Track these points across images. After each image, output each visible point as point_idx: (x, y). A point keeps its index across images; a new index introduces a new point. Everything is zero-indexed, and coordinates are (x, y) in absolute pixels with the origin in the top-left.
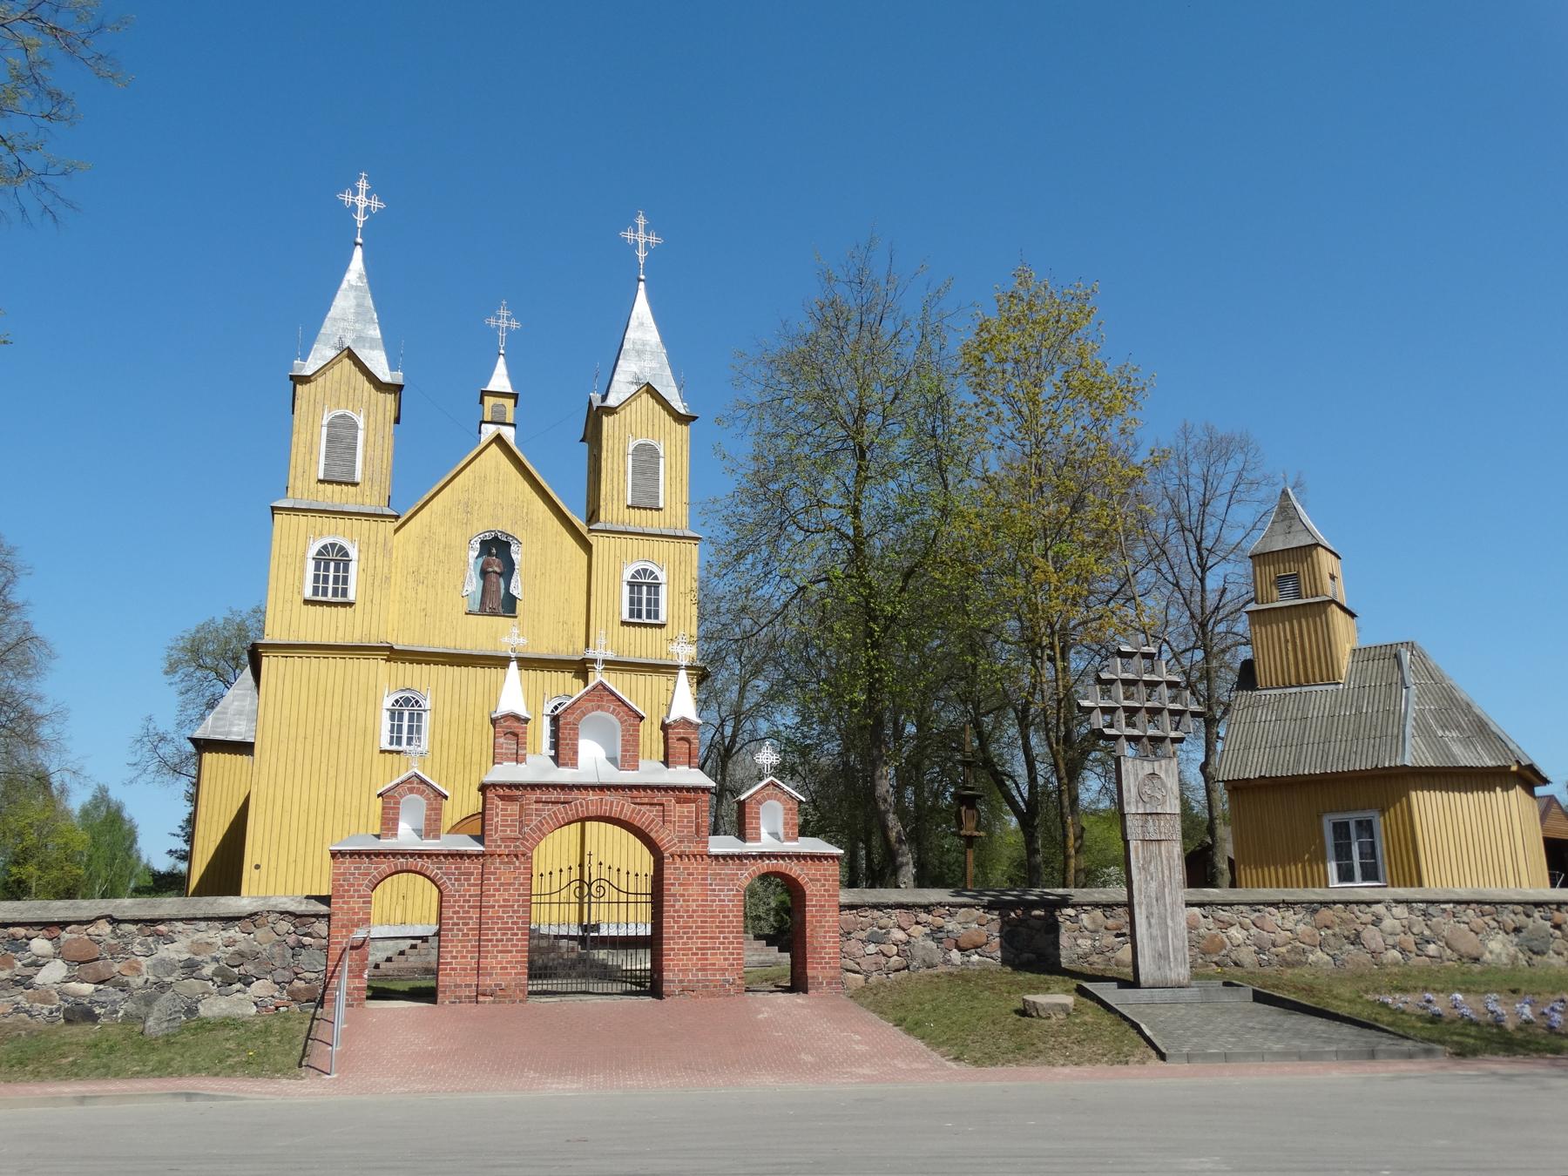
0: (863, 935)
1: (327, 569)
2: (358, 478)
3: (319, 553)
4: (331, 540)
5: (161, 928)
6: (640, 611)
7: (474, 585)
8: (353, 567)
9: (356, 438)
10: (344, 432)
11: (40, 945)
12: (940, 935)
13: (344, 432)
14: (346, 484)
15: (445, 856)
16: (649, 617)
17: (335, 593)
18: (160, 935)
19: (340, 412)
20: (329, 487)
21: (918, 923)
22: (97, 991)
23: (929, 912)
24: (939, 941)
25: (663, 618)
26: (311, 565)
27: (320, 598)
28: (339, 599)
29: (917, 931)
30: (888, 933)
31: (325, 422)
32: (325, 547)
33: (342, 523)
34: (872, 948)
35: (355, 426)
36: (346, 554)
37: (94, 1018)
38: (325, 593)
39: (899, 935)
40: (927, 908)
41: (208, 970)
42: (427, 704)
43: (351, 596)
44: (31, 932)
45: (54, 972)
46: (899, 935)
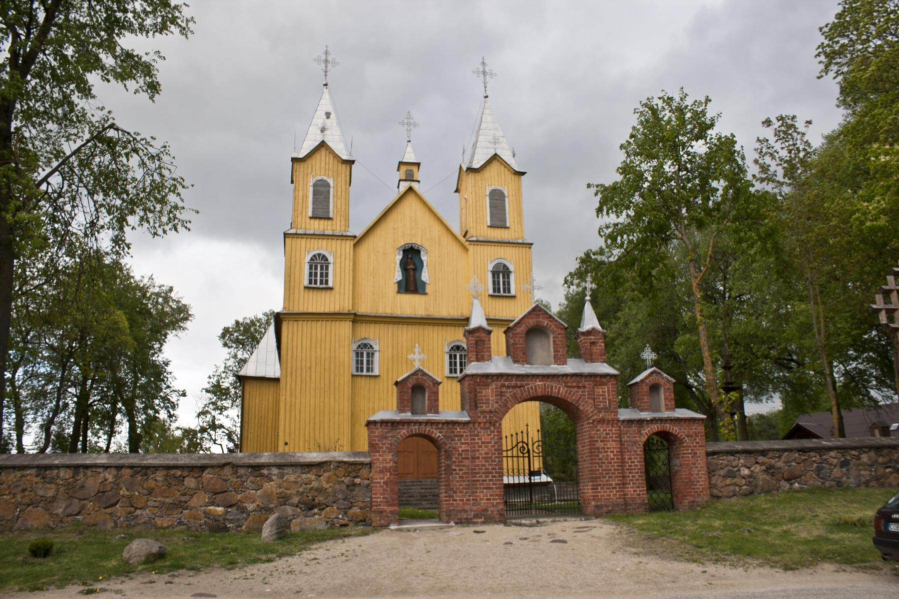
0: (722, 472)
1: (316, 268)
2: (331, 216)
3: (312, 259)
4: (318, 252)
5: (265, 472)
6: (499, 289)
7: (399, 276)
8: (331, 267)
9: (329, 192)
10: (322, 189)
11: (190, 482)
12: (772, 471)
13: (322, 189)
14: (325, 218)
15: (443, 423)
16: (504, 292)
17: (321, 283)
18: (262, 475)
19: (320, 178)
20: (317, 222)
21: (757, 463)
22: (227, 512)
23: (764, 456)
24: (773, 475)
25: (513, 293)
26: (307, 267)
27: (313, 285)
28: (324, 286)
29: (757, 468)
30: (739, 470)
31: (311, 184)
32: (314, 256)
33: (324, 242)
34: (728, 481)
35: (328, 185)
36: (327, 260)
37: (226, 529)
38: (315, 283)
39: (746, 472)
40: (763, 453)
41: (295, 500)
42: (376, 347)
43: (330, 284)
44: (185, 473)
45: (199, 500)
46: (746, 472)
